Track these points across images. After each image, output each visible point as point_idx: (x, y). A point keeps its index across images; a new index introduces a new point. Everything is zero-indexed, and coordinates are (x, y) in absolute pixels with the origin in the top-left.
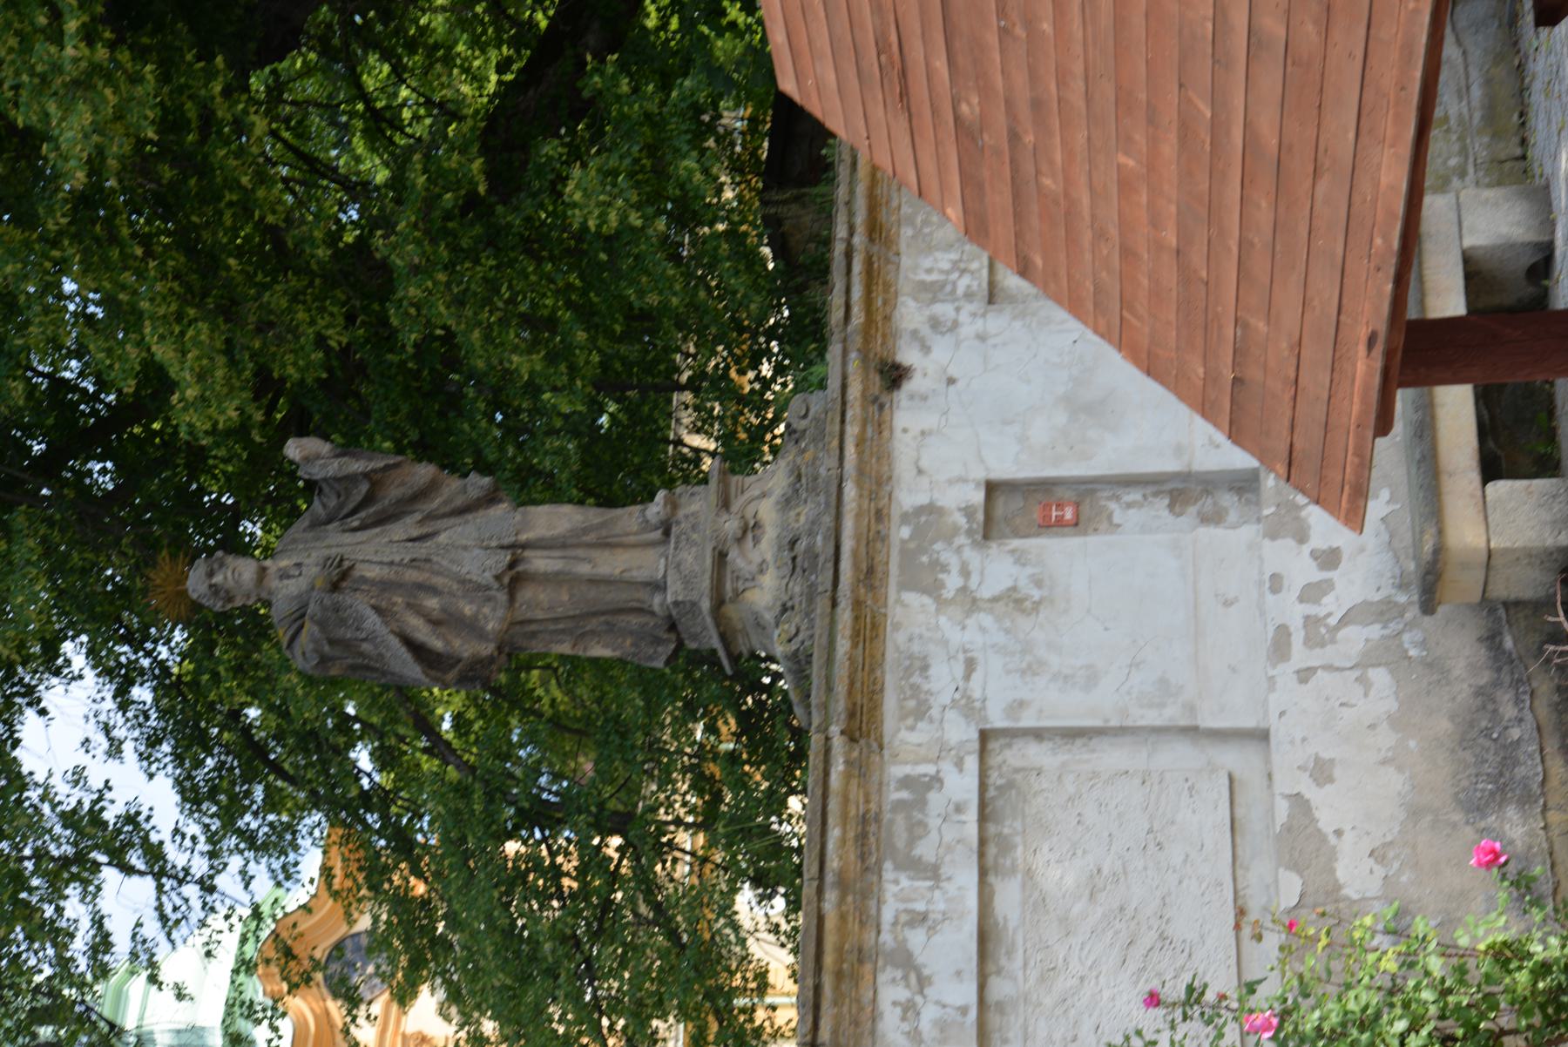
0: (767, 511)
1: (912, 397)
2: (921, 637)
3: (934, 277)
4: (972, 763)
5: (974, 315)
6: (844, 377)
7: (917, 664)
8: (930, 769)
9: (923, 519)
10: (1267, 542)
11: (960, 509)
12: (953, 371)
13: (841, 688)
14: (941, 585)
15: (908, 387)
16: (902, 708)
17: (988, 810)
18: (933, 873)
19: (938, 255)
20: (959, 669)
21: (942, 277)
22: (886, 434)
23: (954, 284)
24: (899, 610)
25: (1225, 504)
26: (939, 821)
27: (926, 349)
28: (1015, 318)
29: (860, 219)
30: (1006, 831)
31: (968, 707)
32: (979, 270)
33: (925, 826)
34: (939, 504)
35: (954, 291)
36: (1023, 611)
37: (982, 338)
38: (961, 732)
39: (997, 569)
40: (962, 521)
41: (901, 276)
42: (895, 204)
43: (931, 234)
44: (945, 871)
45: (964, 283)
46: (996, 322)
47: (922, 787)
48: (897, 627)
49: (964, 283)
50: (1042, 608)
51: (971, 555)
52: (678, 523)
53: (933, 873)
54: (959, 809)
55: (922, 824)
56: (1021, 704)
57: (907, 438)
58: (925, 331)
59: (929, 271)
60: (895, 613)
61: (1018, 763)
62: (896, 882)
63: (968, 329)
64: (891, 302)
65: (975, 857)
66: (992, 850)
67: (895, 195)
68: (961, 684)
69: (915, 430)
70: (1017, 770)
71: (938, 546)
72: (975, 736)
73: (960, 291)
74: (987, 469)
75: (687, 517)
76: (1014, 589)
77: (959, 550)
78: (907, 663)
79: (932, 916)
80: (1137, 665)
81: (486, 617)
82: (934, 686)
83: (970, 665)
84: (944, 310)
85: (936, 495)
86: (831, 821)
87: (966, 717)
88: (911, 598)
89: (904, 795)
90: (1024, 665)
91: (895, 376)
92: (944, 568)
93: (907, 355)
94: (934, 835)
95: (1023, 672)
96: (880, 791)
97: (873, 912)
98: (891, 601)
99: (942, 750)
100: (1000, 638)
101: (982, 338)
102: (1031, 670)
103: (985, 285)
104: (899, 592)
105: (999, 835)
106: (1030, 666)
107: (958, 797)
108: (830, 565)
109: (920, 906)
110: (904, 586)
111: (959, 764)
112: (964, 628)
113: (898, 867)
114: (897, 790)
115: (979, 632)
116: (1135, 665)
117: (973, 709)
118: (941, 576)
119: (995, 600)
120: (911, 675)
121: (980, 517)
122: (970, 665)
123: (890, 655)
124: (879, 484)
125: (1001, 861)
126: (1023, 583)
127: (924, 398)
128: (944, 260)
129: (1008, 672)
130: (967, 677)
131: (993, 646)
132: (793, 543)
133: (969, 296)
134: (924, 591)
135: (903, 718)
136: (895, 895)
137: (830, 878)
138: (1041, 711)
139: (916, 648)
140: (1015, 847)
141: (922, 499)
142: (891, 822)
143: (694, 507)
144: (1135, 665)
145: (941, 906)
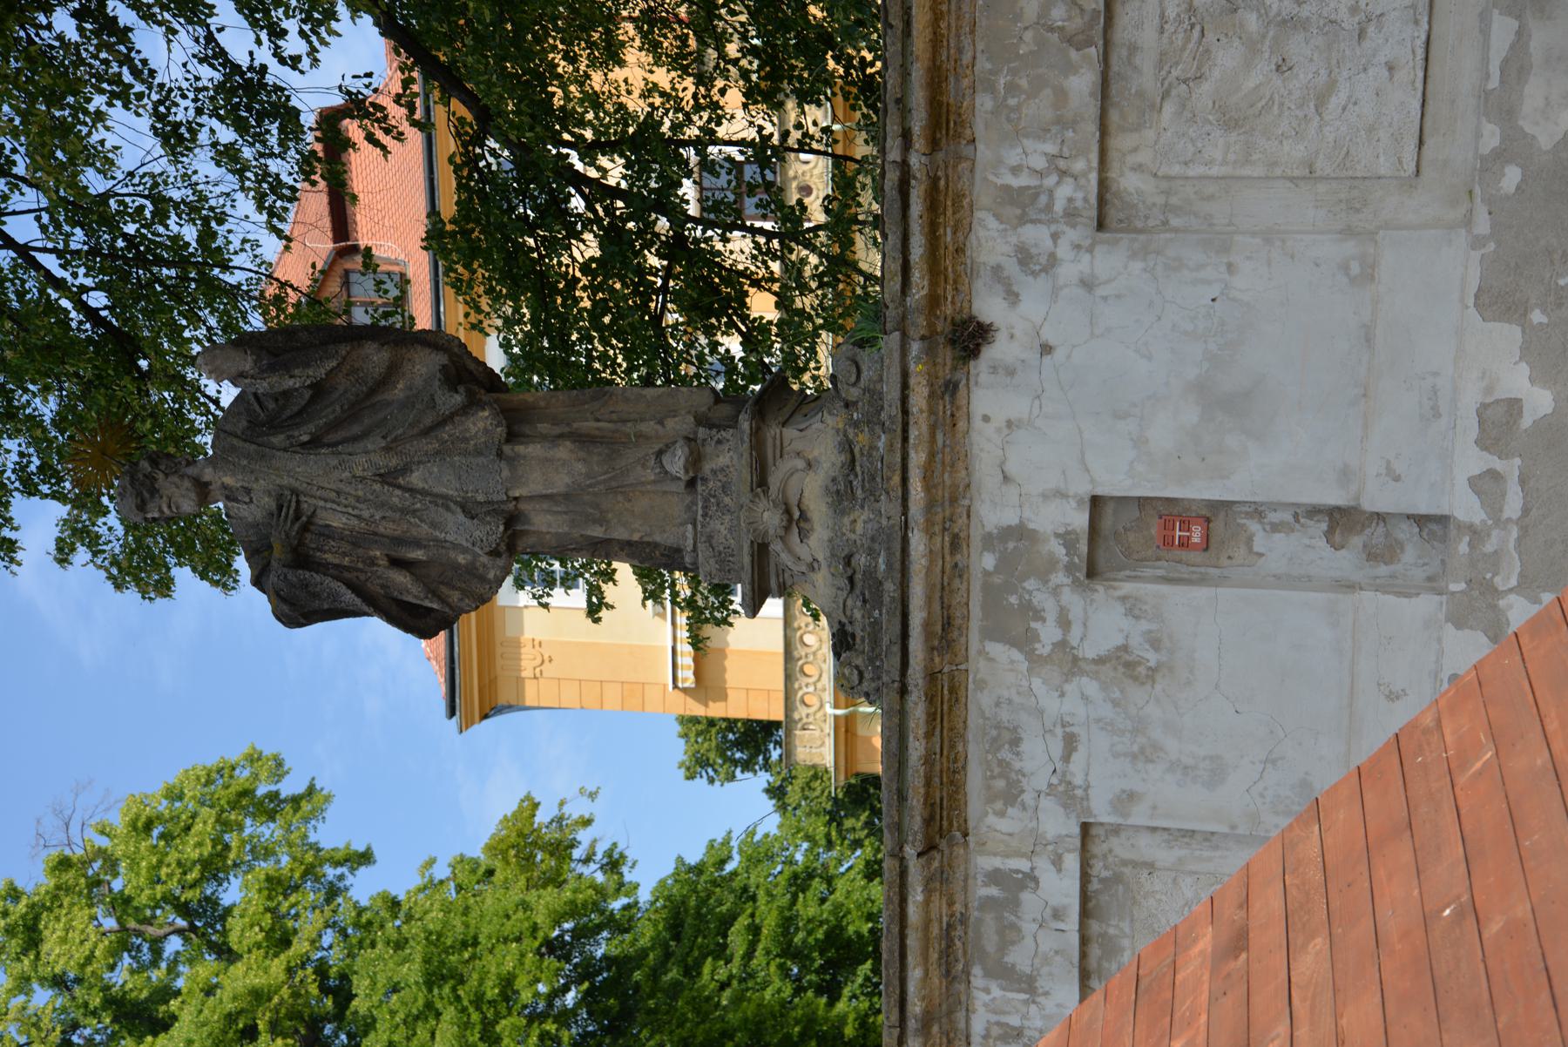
0: (813, 491)
1: (994, 369)
2: (1010, 701)
3: (1023, 181)
4: (1072, 862)
5: (1077, 247)
6: (905, 375)
7: (1006, 735)
8: (1023, 865)
9: (1011, 545)
10: (1450, 627)
11: (1057, 535)
12: (1048, 335)
13: (916, 801)
14: (1032, 637)
15: (989, 354)
16: (989, 788)
17: (1091, 905)
18: (1028, 985)
19: (1029, 143)
20: (1057, 748)
21: (1034, 182)
22: (961, 425)
23: (1051, 192)
24: (982, 664)
25: (1401, 536)
26: (1035, 926)
27: (1013, 297)
28: (1133, 256)
29: (918, 124)
30: (1111, 931)
31: (1068, 795)
32: (1085, 174)
33: (1019, 930)
34: (1031, 526)
35: (1049, 207)
36: (1135, 679)
37: (1088, 284)
38: (1058, 824)
39: (1103, 621)
40: (1060, 551)
41: (978, 176)
42: (966, 58)
43: (1018, 108)
44: (1041, 983)
45: (1065, 191)
46: (1109, 261)
47: (1017, 884)
48: (981, 685)
49: (1065, 191)
50: (1158, 677)
51: (1070, 598)
52: (704, 480)
53: (1028, 985)
54: (1057, 914)
55: (1014, 927)
56: (1132, 797)
57: (989, 429)
58: (1012, 268)
59: (1015, 170)
60: (978, 668)
61: (1127, 855)
62: (987, 991)
63: (1071, 269)
64: (963, 227)
65: (1076, 972)
66: (1095, 951)
67: (966, 41)
68: (1059, 766)
69: (999, 418)
70: (1125, 863)
71: (1030, 584)
72: (1077, 830)
73: (1059, 207)
74: (1092, 481)
75: (714, 472)
76: (1125, 648)
77: (1056, 591)
78: (994, 733)
79: (1027, 1033)
80: (1274, 762)
81: (484, 566)
82: (1027, 765)
83: (1070, 743)
84: (1038, 235)
85: (1027, 514)
86: (911, 959)
87: (1065, 806)
88: (996, 649)
89: (993, 891)
90: (1135, 748)
91: (970, 338)
92: (1039, 616)
93: (988, 306)
94: (1029, 941)
95: (1134, 757)
96: (965, 889)
97: (962, 1025)
98: (972, 652)
99: (1036, 844)
100: (1107, 711)
101: (1088, 284)
102: (1146, 755)
103: (1093, 200)
104: (981, 641)
105: (1104, 935)
106: (1142, 750)
107: (1055, 901)
108: (896, 649)
109: (1014, 1021)
110: (988, 634)
111: (1057, 862)
112: (1062, 695)
113: (988, 974)
114: (986, 885)
115: (1078, 702)
116: (1271, 761)
117: (1073, 797)
118: (1033, 625)
119: (1100, 661)
120: (998, 749)
121: (1083, 548)
122: (1070, 743)
123: (973, 720)
124: (954, 500)
125: (1106, 965)
126: (1136, 641)
127: (1011, 372)
128: (1037, 153)
129: (1116, 755)
130: (1066, 758)
131: (1098, 721)
132: (848, 560)
133: (1071, 215)
134: (1013, 643)
135: (990, 800)
136: (985, 1005)
137: (912, 1024)
138: (1154, 808)
139: (1004, 715)
140: (1122, 950)
141: (1010, 518)
142: (980, 921)
143: (723, 460)
144: (1271, 761)
145: (1038, 1023)
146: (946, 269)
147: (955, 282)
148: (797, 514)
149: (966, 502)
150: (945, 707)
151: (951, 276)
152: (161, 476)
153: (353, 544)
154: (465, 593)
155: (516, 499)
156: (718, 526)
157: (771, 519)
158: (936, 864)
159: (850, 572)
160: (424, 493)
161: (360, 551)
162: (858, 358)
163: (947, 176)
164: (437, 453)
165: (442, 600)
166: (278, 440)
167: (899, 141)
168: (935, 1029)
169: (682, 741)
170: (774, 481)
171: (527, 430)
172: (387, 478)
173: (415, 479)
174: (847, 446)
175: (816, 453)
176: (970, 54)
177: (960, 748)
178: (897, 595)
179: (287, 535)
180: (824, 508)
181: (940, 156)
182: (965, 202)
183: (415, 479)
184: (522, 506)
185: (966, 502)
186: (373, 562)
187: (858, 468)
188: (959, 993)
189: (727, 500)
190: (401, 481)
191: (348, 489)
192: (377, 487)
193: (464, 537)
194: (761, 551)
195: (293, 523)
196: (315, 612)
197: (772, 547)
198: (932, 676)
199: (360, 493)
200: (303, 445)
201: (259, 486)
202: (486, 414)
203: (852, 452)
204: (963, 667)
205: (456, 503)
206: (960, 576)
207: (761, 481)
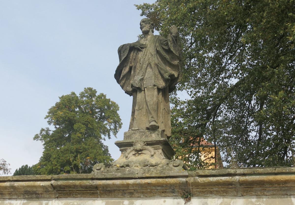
0: (145, 157)
97: (14, 197)
108: (103, 177)
124: (143, 193)
132: (128, 166)
146: (206, 188)
147: (202, 192)
148: (140, 153)
149: (142, 196)
150: (88, 191)
151: (204, 190)
152: (150, 25)
153: (135, 59)
154: (124, 84)
155: (144, 90)
156: (137, 135)
157: (139, 146)
158: (50, 189)
159: (125, 166)
160: (146, 71)
162: (180, 166)
163: (232, 188)
164: (155, 74)
166: (157, 44)
167: (242, 172)
168: (12, 190)
170: (148, 147)
171: (161, 93)
172: (149, 64)
173: (149, 70)
174: (156, 165)
175: (155, 157)
176: (267, 194)
177: (79, 196)
178: (117, 176)
179: (136, 45)
180: (141, 159)
181: (238, 186)
182: (225, 194)
183: (149, 70)
185: (142, 196)
186: (131, 63)
187: (151, 167)
188: (20, 196)
189: (144, 137)
190: (148, 67)
191: (147, 57)
192: (147, 62)
193: (136, 80)
194: (130, 145)
195: (139, 46)
196: (121, 54)
197: (132, 147)
198: (96, 187)
199: (146, 59)
200: (156, 49)
201: (147, 42)
203: (155, 166)
204: (99, 196)
205: (144, 77)
206: (122, 195)
207: (149, 144)
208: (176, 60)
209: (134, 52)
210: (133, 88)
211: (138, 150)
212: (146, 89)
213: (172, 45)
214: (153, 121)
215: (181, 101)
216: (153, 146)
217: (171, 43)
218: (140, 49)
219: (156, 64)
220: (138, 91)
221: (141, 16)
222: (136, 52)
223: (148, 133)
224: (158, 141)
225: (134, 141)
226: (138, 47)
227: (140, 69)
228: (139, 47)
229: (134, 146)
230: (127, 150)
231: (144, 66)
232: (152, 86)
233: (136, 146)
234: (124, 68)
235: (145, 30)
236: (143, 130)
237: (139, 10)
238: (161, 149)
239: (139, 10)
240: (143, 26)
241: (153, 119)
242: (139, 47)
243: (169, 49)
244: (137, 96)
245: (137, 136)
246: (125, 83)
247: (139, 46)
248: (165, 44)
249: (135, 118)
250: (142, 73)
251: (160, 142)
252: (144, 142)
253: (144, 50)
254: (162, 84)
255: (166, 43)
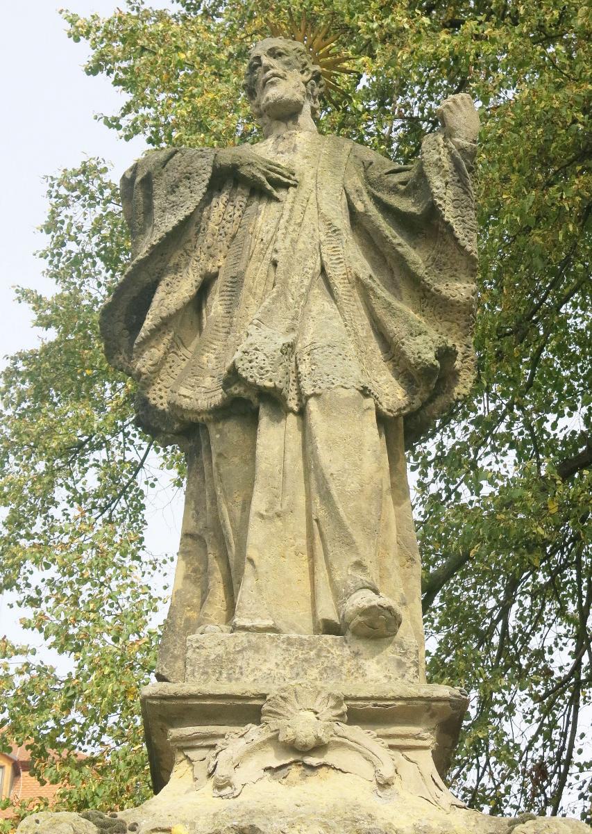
48: (364, 606)
148: (313, 760)
155: (302, 413)
157: (304, 724)
161: (222, 246)
165: (157, 331)
166: (356, 181)
169: (78, 167)
170: (356, 732)
175: (403, 794)
183: (320, 304)
184: (292, 420)
189: (314, 673)
191: (304, 238)
199: (300, 246)
202: (400, 397)
205: (296, 340)
207: (364, 713)
208: (454, 277)
209: (228, 201)
210: (236, 390)
211: (305, 746)
212: (313, 405)
213: (450, 193)
214: (367, 588)
215: (16, 648)
216: (382, 730)
217: (447, 183)
218: (269, 187)
219: (358, 279)
220: (262, 411)
221: (88, 74)
222: (240, 200)
223: (336, 651)
224: (420, 698)
225: (272, 690)
226: (259, 175)
227: (278, 296)
228: (263, 178)
229: (274, 723)
230: (219, 742)
231: (296, 279)
232: (353, 393)
233: (284, 721)
234: (168, 279)
235: (287, 96)
236: (300, 632)
237: (77, 40)
238: (426, 748)
239: (77, 40)
240: (274, 75)
241: (360, 576)
242: (263, 178)
243: (433, 212)
244: (260, 441)
245: (272, 666)
246: (163, 361)
247: (265, 174)
248: (402, 188)
249: (251, 561)
250: (290, 314)
251: (429, 709)
252: (339, 701)
253: (286, 196)
254: (393, 395)
255: (403, 183)
